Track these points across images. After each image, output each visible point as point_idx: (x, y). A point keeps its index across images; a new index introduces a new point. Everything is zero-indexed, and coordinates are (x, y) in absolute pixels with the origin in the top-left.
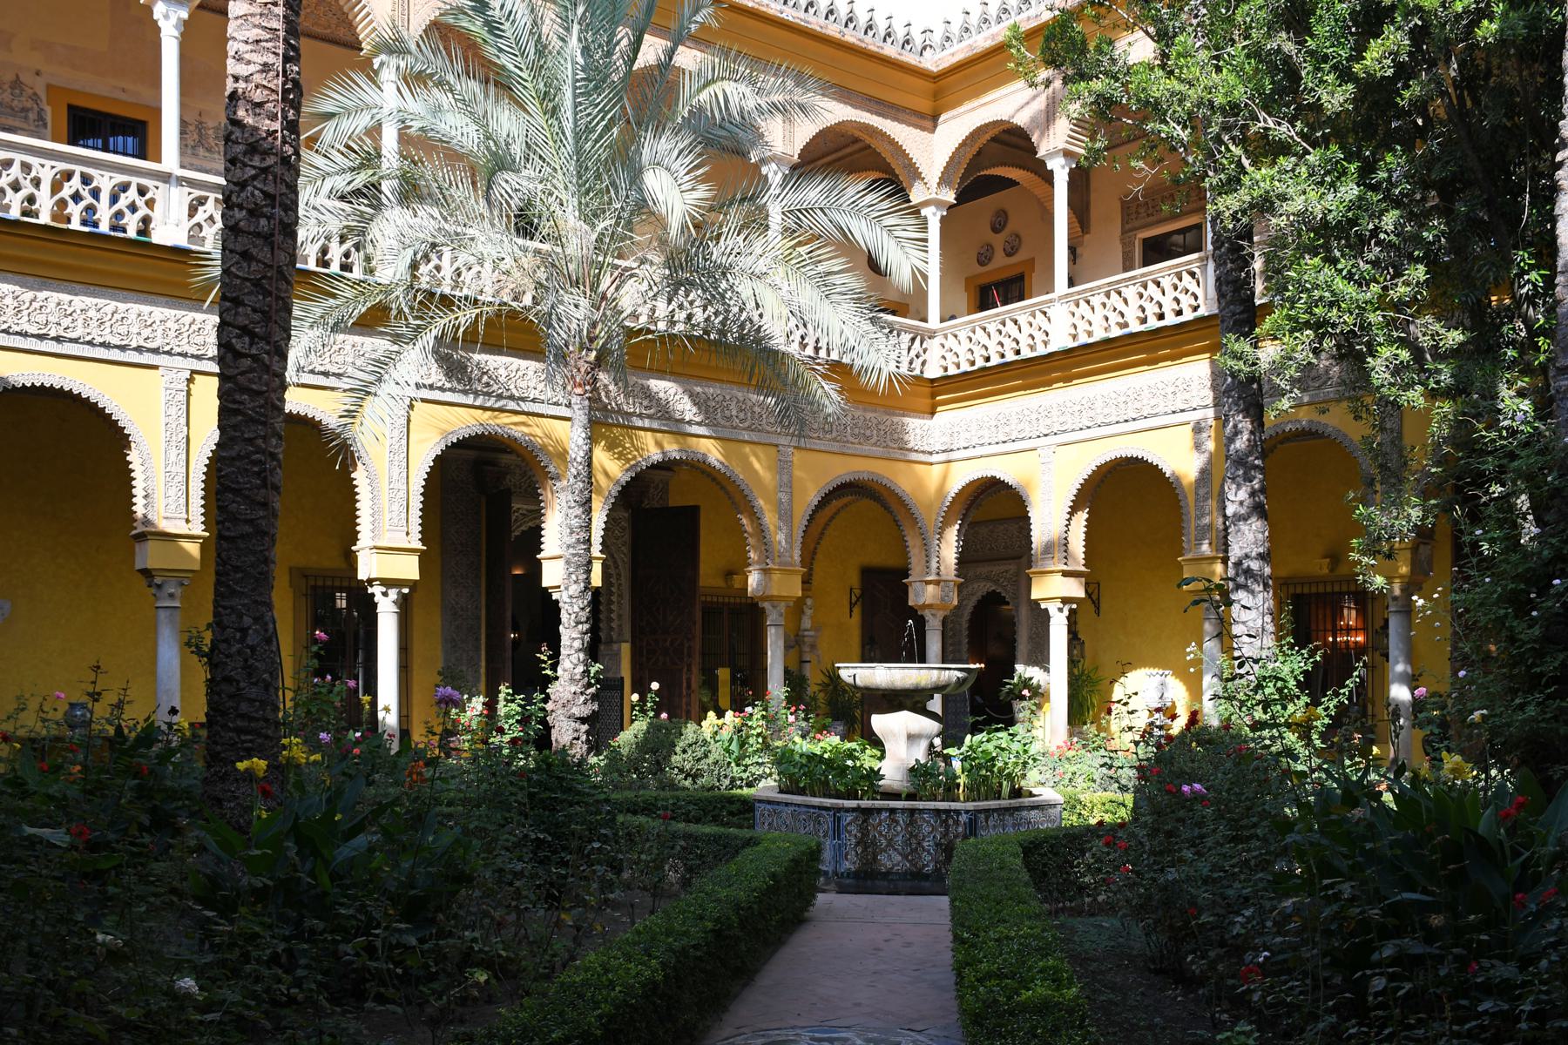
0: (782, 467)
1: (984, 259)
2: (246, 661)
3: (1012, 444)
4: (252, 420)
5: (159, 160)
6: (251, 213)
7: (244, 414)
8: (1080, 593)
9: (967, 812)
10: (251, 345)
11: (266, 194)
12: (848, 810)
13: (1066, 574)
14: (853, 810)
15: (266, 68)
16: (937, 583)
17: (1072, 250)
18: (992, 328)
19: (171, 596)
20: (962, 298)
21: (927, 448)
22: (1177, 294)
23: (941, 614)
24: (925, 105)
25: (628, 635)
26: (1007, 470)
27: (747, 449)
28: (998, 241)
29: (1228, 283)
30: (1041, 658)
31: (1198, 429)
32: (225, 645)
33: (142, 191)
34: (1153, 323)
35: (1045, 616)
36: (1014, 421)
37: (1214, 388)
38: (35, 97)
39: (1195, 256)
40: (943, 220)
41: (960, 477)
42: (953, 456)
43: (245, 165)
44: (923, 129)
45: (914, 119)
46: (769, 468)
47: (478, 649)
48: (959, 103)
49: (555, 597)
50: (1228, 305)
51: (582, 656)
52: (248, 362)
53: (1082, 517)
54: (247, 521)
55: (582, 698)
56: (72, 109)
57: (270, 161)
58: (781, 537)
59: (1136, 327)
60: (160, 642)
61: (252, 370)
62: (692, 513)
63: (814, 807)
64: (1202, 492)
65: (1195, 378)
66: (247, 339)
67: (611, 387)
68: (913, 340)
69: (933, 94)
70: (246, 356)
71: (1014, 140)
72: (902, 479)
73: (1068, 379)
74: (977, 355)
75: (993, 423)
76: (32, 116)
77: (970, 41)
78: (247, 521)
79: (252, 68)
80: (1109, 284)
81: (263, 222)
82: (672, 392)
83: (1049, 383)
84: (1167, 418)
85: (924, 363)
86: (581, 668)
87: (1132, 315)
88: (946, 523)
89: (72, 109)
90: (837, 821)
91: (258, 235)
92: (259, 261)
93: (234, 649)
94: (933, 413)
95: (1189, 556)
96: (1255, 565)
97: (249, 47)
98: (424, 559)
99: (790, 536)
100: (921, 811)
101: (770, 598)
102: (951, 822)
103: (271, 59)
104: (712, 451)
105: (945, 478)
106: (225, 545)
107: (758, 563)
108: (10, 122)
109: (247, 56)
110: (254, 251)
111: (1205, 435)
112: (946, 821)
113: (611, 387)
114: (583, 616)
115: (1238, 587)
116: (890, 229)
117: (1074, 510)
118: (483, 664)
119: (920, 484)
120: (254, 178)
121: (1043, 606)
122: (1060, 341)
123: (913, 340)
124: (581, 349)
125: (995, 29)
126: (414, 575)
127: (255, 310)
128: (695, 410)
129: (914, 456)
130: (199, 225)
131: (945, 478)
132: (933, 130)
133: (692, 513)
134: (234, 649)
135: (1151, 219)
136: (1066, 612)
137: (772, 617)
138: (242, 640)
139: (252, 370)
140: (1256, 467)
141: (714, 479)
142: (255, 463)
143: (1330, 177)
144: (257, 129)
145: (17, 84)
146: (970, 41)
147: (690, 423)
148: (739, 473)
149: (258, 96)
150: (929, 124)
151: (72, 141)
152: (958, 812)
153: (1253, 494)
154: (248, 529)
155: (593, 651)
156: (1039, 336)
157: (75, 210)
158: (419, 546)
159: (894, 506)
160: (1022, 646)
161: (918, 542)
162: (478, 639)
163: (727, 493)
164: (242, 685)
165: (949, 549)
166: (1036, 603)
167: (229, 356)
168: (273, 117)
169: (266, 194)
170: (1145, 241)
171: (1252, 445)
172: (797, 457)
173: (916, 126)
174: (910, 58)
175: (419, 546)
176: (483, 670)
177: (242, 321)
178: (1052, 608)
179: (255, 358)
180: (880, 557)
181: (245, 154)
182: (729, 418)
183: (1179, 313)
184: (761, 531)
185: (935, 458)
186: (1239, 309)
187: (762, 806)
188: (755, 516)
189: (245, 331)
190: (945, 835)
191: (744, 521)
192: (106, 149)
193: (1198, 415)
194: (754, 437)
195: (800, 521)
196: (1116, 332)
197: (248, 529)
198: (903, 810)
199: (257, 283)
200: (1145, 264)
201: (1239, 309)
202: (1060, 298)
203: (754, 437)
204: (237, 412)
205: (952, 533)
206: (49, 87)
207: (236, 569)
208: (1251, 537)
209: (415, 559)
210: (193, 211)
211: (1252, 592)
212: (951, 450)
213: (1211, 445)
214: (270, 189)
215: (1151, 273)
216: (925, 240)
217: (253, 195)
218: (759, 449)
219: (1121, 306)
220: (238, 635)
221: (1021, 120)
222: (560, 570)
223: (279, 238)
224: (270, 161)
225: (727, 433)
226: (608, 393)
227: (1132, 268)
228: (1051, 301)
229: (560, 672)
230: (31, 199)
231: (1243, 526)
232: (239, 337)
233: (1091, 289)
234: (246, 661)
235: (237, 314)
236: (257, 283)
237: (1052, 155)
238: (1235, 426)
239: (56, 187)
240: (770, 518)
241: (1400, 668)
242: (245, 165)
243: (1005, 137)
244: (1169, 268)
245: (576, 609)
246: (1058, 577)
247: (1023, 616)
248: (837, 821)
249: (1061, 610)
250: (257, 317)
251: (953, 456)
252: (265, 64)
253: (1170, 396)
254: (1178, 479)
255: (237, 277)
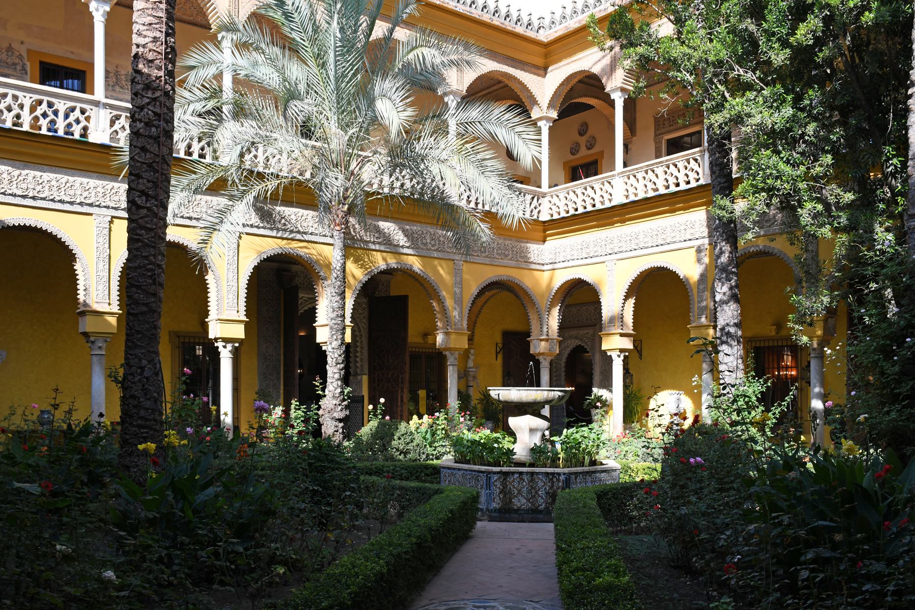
0: (457, 273)
1: (574, 151)
2: (144, 386)
3: (590, 259)
4: (147, 245)
5: (93, 94)
6: (147, 124)
7: (142, 242)
8: (630, 346)
9: (564, 474)
10: (146, 201)
11: (155, 113)
12: (495, 473)
13: (622, 335)
14: (498, 473)
15: (155, 40)
16: (547, 340)
17: (626, 146)
18: (579, 191)
19: (100, 348)
20: (561, 174)
21: (541, 262)
22: (687, 172)
23: (549, 359)
24: (540, 61)
25: (366, 371)
26: (587, 274)
27: (436, 262)
28: (583, 141)
29: (717, 165)
30: (607, 384)
31: (699, 250)
32: (131, 377)
33: (83, 112)
34: (673, 189)
35: (610, 359)
36: (592, 246)
37: (708, 226)
38: (20, 57)
39: (697, 149)
40: (550, 128)
41: (560, 278)
42: (556, 266)
43: (143, 96)
44: (539, 75)
45: (533, 70)
46: (449, 273)
47: (279, 379)
48: (560, 60)
49: (324, 348)
50: (716, 178)
51: (339, 383)
52: (144, 211)
53: (631, 302)
54: (144, 304)
55: (340, 408)
56: (42, 63)
57: (158, 94)
58: (455, 313)
59: (663, 191)
60: (94, 375)
61: (147, 216)
62: (404, 300)
63: (475, 471)
64: (701, 287)
65: (697, 220)
66: (144, 198)
67: (357, 226)
68: (533, 198)
69: (545, 55)
70: (143, 208)
71: (592, 82)
72: (527, 280)
73: (623, 221)
74: (570, 207)
75: (580, 247)
76: (19, 68)
77: (566, 24)
78: (144, 304)
79: (147, 40)
80: (647, 166)
81: (154, 129)
82: (392, 229)
83: (612, 224)
84: (681, 244)
85: (539, 212)
86: (339, 390)
87: (661, 184)
88: (552, 305)
89: (42, 63)
90: (489, 479)
91: (151, 137)
92: (151, 153)
93: (136, 379)
94: (544, 241)
95: (694, 325)
96: (732, 330)
97: (145, 28)
98: (248, 326)
99: (461, 313)
100: (538, 473)
101: (449, 349)
102: (555, 480)
103: (158, 34)
104: (415, 263)
105: (551, 279)
106: (131, 318)
107: (442, 328)
108: (6, 71)
109: (144, 33)
110: (148, 147)
111: (703, 254)
112: (552, 479)
113: (357, 226)
114: (340, 359)
115: (723, 343)
116: (519, 134)
117: (627, 298)
118: (282, 387)
119: (537, 283)
120: (148, 104)
121: (609, 354)
122: (619, 199)
123: (533, 198)
124: (339, 204)
125: (581, 17)
126: (242, 335)
127: (149, 181)
128: (405, 239)
129: (533, 266)
130: (116, 132)
131: (551, 279)
132: (544, 76)
133: (404, 300)
134: (136, 379)
135: (672, 128)
136: (622, 358)
137: (451, 360)
138: (141, 374)
139: (147, 216)
140: (733, 273)
141: (417, 280)
142: (149, 270)
143: (776, 103)
144: (150, 75)
145: (10, 49)
146: (566, 24)
147: (402, 247)
148: (432, 276)
149: (151, 56)
150: (542, 72)
151: (42, 83)
152: (559, 474)
153: (731, 288)
154: (145, 309)
155: (346, 380)
156: (607, 196)
157: (44, 123)
158: (245, 319)
159: (522, 296)
160: (597, 377)
161: (536, 316)
162: (279, 373)
163: (424, 288)
164: (141, 400)
165: (554, 320)
166: (605, 352)
167: (134, 208)
168: (159, 68)
169: (155, 113)
170: (668, 140)
171: (731, 260)
172: (465, 267)
173: (535, 74)
174: (531, 34)
175: (245, 319)
176: (282, 391)
177: (141, 187)
178: (614, 355)
179: (149, 209)
180: (514, 325)
181: (143, 90)
182: (426, 244)
183: (688, 183)
184: (444, 310)
185: (546, 267)
186: (723, 180)
187: (445, 470)
188: (441, 301)
189: (143, 193)
190: (551, 487)
191: (434, 304)
192: (62, 87)
193: (699, 242)
194: (440, 255)
195: (467, 304)
196: (651, 194)
197: (145, 309)
198: (527, 473)
199: (150, 165)
200: (668, 154)
201: (723, 180)
202: (619, 174)
203: (440, 255)
204: (138, 240)
205: (556, 311)
206: (29, 51)
207: (138, 332)
208: (730, 313)
209: (242, 327)
210: (112, 123)
211: (731, 346)
212: (555, 263)
213: (706, 260)
214: (158, 110)
215: (671, 159)
216: (540, 140)
217: (147, 114)
218: (443, 262)
219: (654, 179)
220: (139, 371)
221: (596, 70)
222: (327, 333)
223: (163, 139)
224: (158, 94)
225: (424, 253)
226: (355, 229)
227: (660, 156)
228: (613, 176)
229: (327, 392)
230: (18, 116)
231: (725, 307)
232: (139, 197)
233: (637, 169)
234: (144, 386)
235: (138, 183)
236: (150, 165)
237: (614, 90)
238: (721, 249)
239: (33, 109)
240: (449, 303)
241: (817, 390)
242: (143, 96)
243: (587, 80)
244: (682, 156)
245: (336, 355)
246: (618, 337)
247: (597, 359)
248: (489, 479)
249: (619, 356)
250: (150, 185)
251: (556, 266)
252: (155, 38)
253: (683, 231)
254: (687, 279)
255: (138, 162)
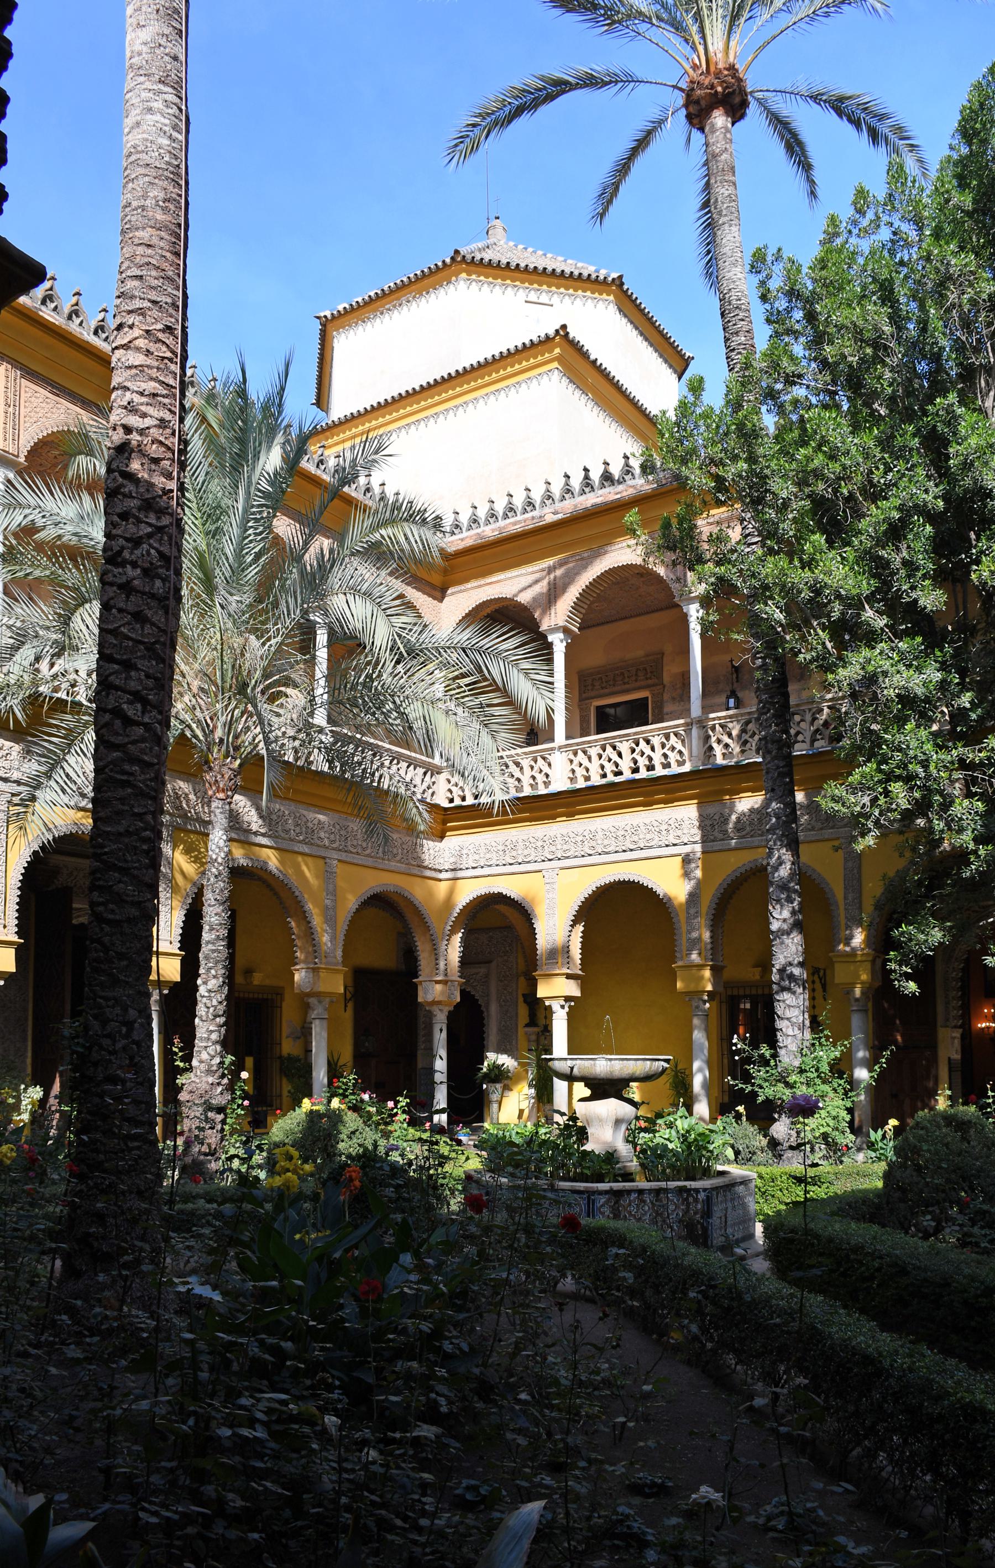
0: (328, 876)
2: (132, 1058)
3: (518, 866)
4: (143, 794)
6: (146, 572)
7: (134, 786)
8: (577, 993)
9: (705, 1190)
10: (143, 713)
11: (162, 555)
13: (569, 976)
14: (606, 1192)
15: (163, 423)
16: (444, 982)
21: (437, 867)
22: (665, 750)
23: (447, 1009)
24: (436, 579)
26: (511, 887)
27: (300, 859)
29: (773, 742)
31: (687, 860)
32: (108, 1041)
35: (549, 1011)
36: (482, 850)
37: (701, 827)
39: (682, 721)
41: (467, 893)
42: (460, 874)
43: (139, 521)
44: (434, 598)
45: (428, 589)
46: (317, 877)
47: (25, 1040)
48: (466, 580)
50: (773, 759)
51: (219, 1048)
52: (141, 730)
53: (580, 928)
54: (133, 904)
55: (219, 1089)
57: (166, 521)
58: (325, 938)
61: (143, 740)
64: (692, 911)
65: (686, 819)
66: (139, 706)
67: (192, 797)
68: (425, 774)
70: (138, 724)
72: (417, 891)
73: (571, 815)
74: (455, 795)
75: (501, 848)
77: (479, 531)
78: (133, 904)
79: (148, 422)
80: (605, 739)
81: (158, 583)
82: (242, 804)
83: (553, 817)
84: (661, 851)
85: (433, 794)
86: (217, 1060)
87: (626, 765)
88: (453, 931)
91: (153, 596)
92: (153, 624)
93: (119, 1045)
94: (442, 837)
95: (680, 963)
96: (797, 971)
97: (144, 400)
98: (21, 953)
99: (333, 939)
100: (666, 1190)
101: (318, 995)
102: (691, 1199)
103: (168, 416)
104: (272, 859)
105: (451, 892)
107: (305, 962)
109: (143, 408)
110: (149, 613)
111: (693, 865)
112: (687, 1199)
113: (192, 797)
114: (221, 1008)
115: (783, 989)
116: (526, 673)
117: (575, 923)
118: (29, 1054)
119: (431, 894)
120: (150, 536)
121: (547, 1003)
122: (560, 783)
123: (425, 774)
124: (226, 756)
125: (501, 523)
126: (11, 967)
127: (148, 676)
128: (260, 822)
129: (428, 873)
131: (451, 892)
132: (441, 600)
134: (119, 1045)
135: (602, 691)
136: (567, 1009)
138: (127, 1036)
139: (143, 740)
140: (795, 891)
141: (268, 886)
143: (912, 662)
144: (153, 485)
146: (479, 531)
147: (256, 833)
148: (293, 880)
149: (155, 451)
150: (438, 594)
152: (697, 1191)
153: (793, 913)
154: (134, 912)
156: (540, 778)
159: (409, 915)
160: (492, 1034)
161: (428, 947)
162: (25, 1031)
163: (279, 898)
165: (454, 950)
166: (541, 1000)
168: (169, 476)
169: (162, 555)
171: (792, 875)
172: (340, 869)
173: (430, 595)
175: (15, 938)
177: (133, 685)
178: (556, 1006)
179: (145, 725)
181: (139, 509)
182: (287, 831)
184: (310, 933)
185: (443, 875)
186: (782, 764)
188: (304, 917)
190: (686, 1212)
191: (293, 924)
193: (687, 849)
194: (306, 849)
195: (342, 926)
197: (134, 912)
198: (650, 1191)
199: (150, 648)
201: (782, 764)
202: (560, 748)
203: (306, 849)
205: (457, 939)
207: (121, 956)
208: (794, 949)
209: (11, 953)
211: (794, 993)
212: (464, 868)
213: (698, 873)
215: (643, 732)
216: (552, 683)
217: (148, 553)
218: (309, 860)
219: (585, 762)
220: (124, 1030)
221: (525, 598)
224: (166, 521)
225: (285, 845)
226: (188, 801)
228: (552, 749)
229: (195, 1063)
231: (788, 941)
232: (130, 703)
233: (589, 742)
234: (132, 1058)
235: (128, 678)
236: (150, 648)
237: (555, 630)
238: (779, 857)
240: (317, 921)
241: (861, 1054)
242: (139, 521)
244: (659, 729)
245: (215, 1002)
246: (563, 980)
249: (563, 1007)
250: (150, 683)
251: (460, 874)
252: (162, 420)
253: (664, 833)
254: (670, 899)
